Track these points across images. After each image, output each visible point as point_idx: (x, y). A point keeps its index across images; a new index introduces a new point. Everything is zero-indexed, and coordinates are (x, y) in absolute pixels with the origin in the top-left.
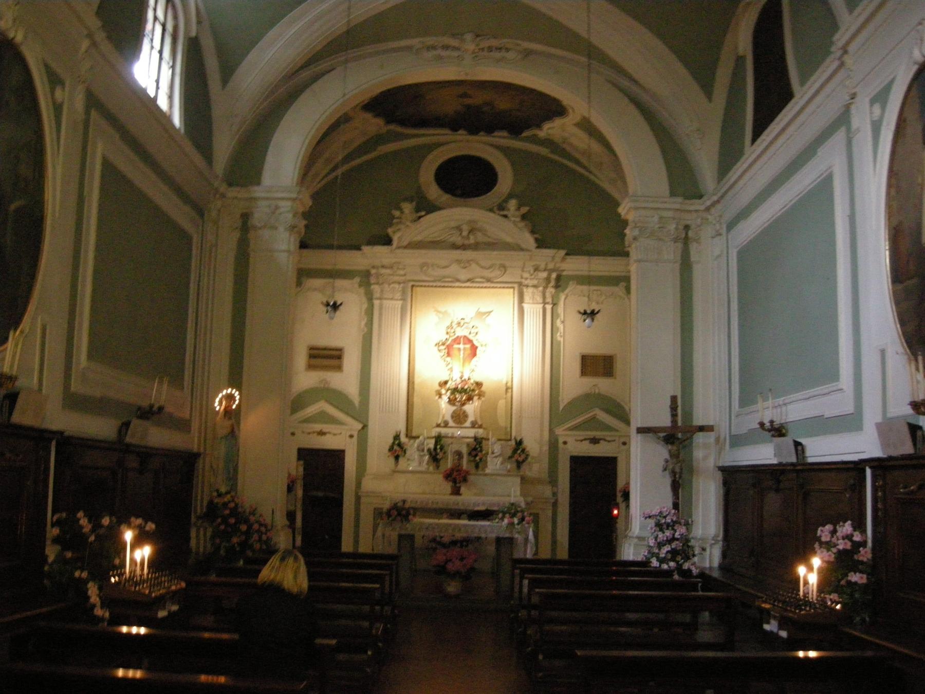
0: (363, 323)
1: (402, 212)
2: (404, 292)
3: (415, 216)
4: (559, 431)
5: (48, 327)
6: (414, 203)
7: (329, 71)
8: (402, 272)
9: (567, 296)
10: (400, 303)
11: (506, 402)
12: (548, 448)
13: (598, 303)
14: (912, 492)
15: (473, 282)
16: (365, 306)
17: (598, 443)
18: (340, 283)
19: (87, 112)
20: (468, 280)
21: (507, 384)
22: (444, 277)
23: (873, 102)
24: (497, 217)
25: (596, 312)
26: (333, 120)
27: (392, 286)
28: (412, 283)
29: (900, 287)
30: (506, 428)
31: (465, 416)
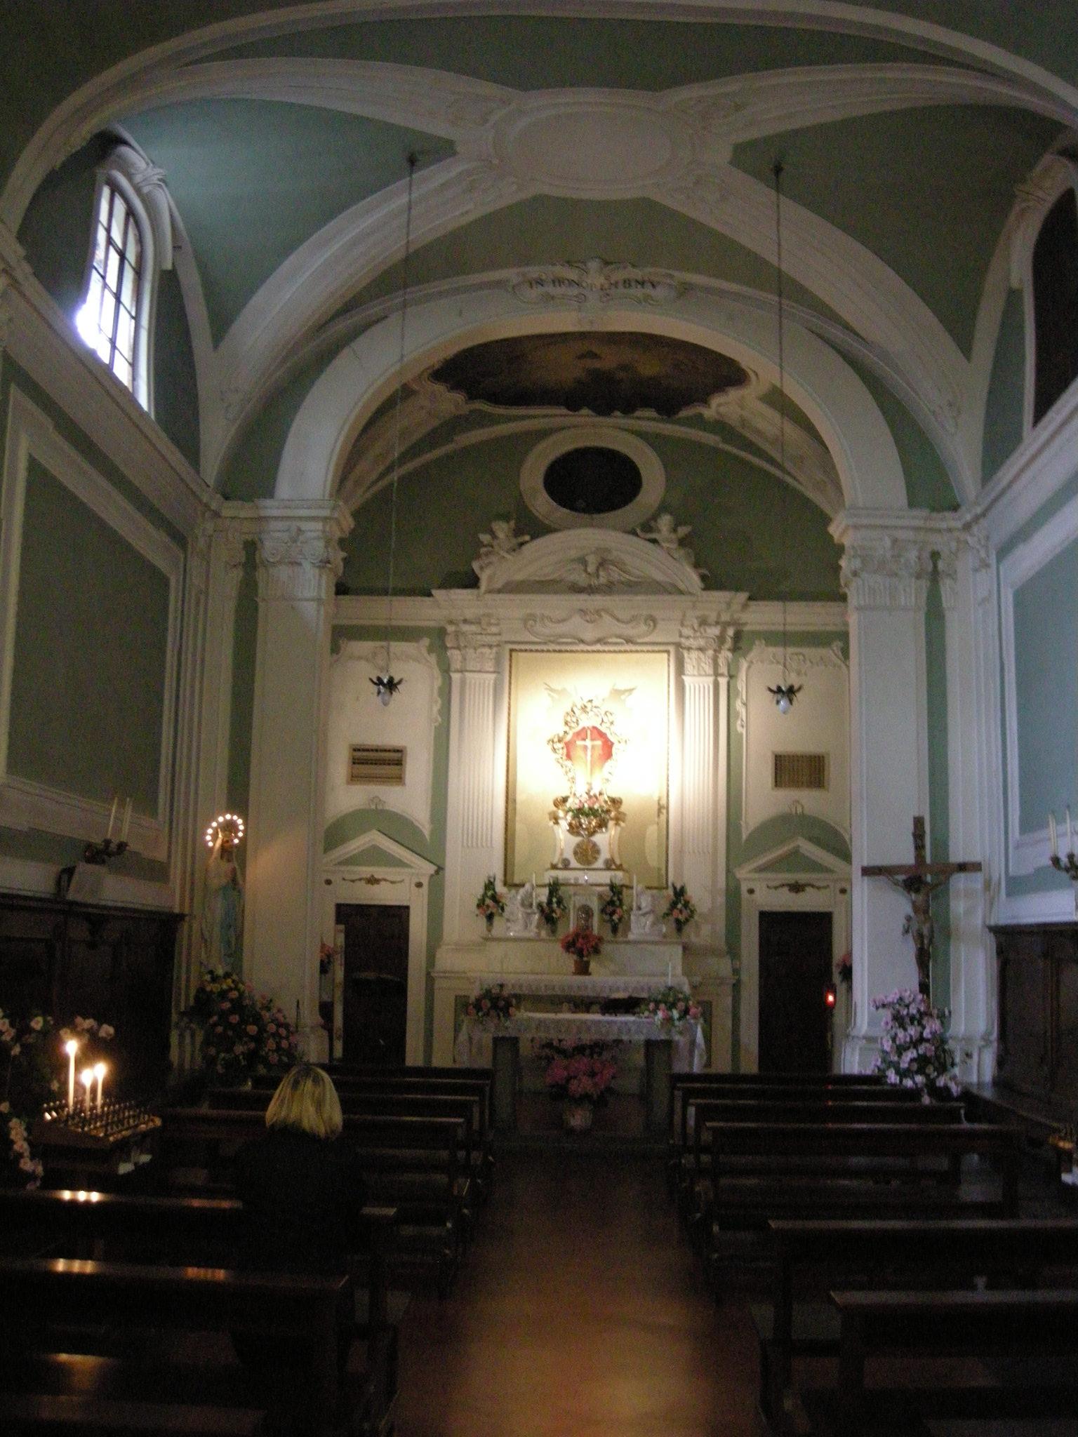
0: (436, 709)
31: (596, 850)
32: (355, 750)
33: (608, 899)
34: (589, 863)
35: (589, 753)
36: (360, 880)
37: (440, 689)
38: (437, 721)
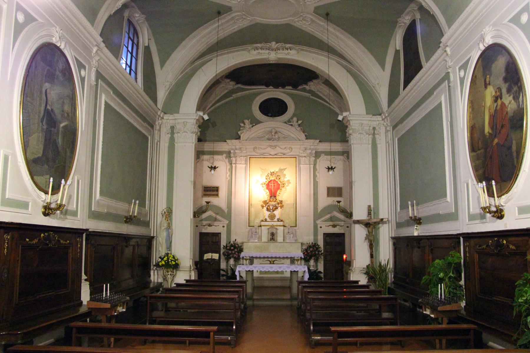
1: (244, 124)
2: (246, 161)
3: (251, 126)
4: (318, 222)
5: (80, 181)
6: (250, 120)
7: (210, 61)
8: (245, 152)
9: (320, 160)
10: (245, 165)
13: (334, 164)
14: (483, 249)
15: (278, 155)
17: (336, 227)
18: (216, 157)
19: (97, 81)
20: (276, 155)
22: (265, 153)
23: (460, 69)
24: (288, 125)
25: (333, 168)
26: (211, 84)
27: (241, 158)
28: (249, 156)
29: (475, 154)
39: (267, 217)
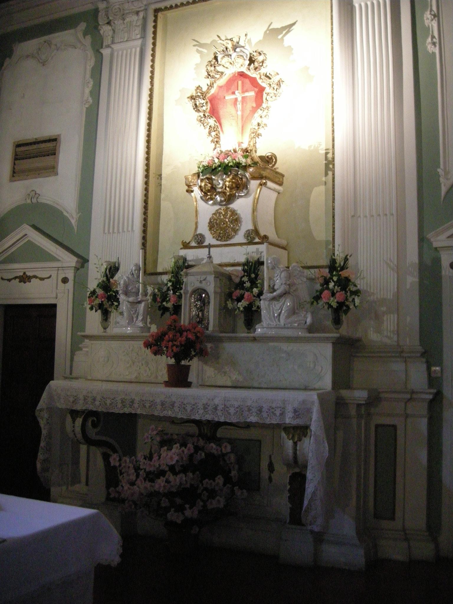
0: (87, 91)
11: (327, 191)
12: (416, 280)
16: (91, 63)
21: (327, 154)
30: (327, 243)
31: (236, 220)
32: (18, 146)
33: (237, 280)
34: (229, 237)
35: (239, 106)
36: (16, 278)
37: (93, 69)
38: (87, 101)
39: (204, 229)
